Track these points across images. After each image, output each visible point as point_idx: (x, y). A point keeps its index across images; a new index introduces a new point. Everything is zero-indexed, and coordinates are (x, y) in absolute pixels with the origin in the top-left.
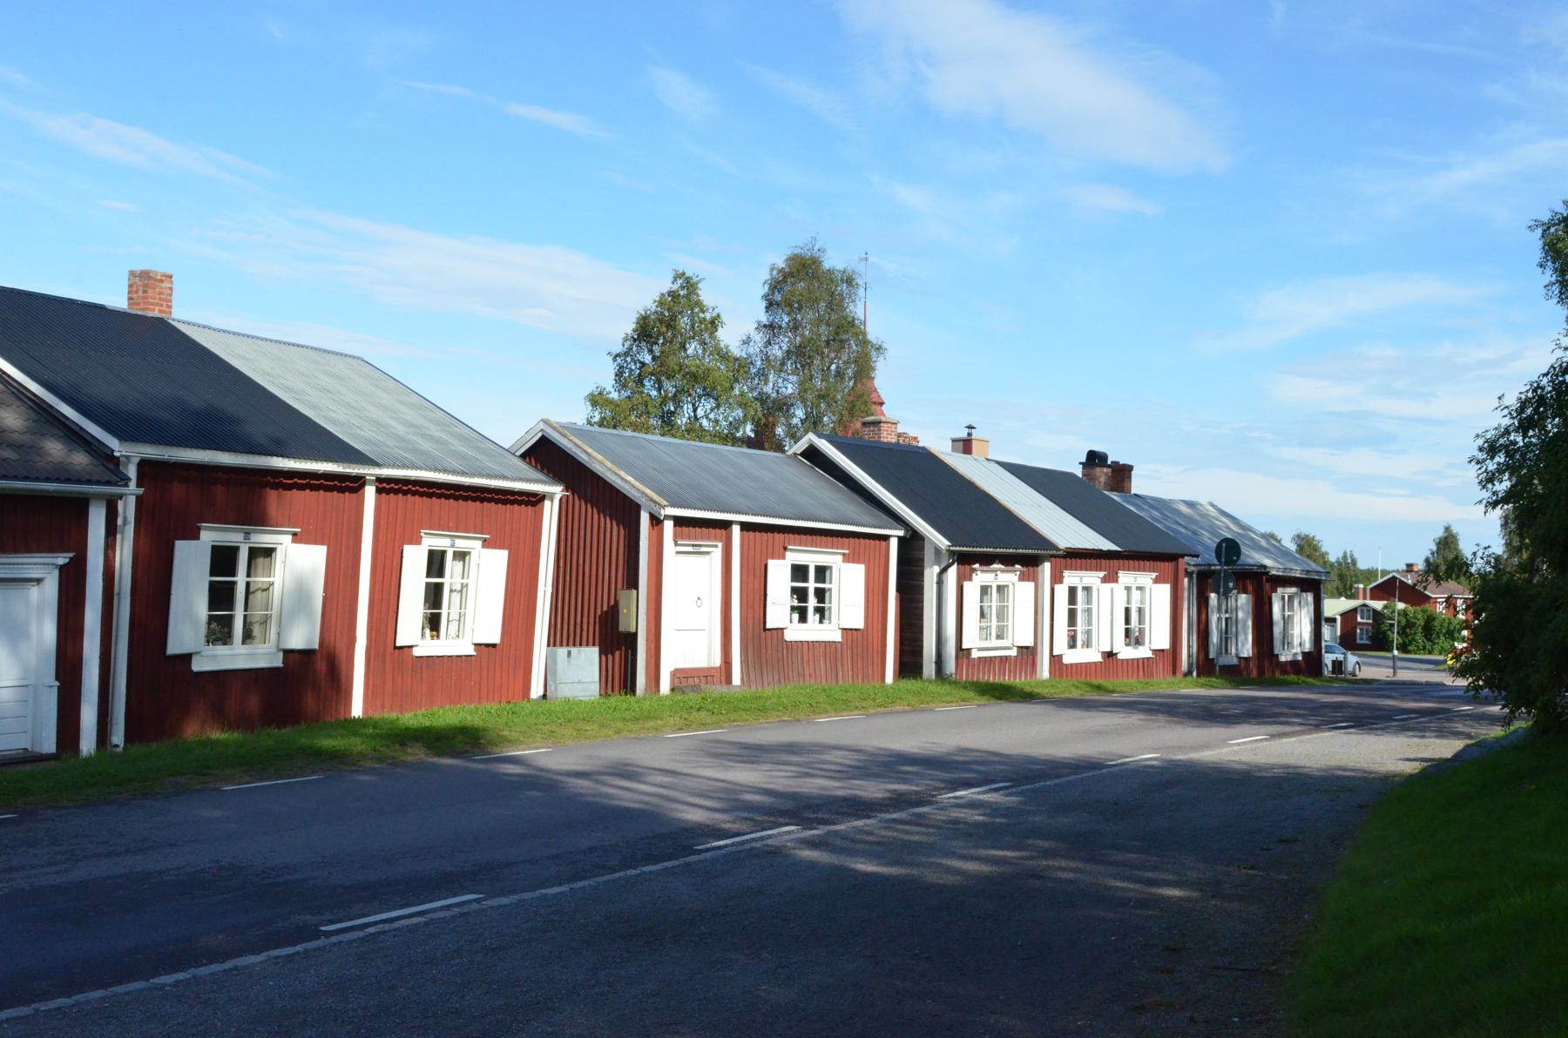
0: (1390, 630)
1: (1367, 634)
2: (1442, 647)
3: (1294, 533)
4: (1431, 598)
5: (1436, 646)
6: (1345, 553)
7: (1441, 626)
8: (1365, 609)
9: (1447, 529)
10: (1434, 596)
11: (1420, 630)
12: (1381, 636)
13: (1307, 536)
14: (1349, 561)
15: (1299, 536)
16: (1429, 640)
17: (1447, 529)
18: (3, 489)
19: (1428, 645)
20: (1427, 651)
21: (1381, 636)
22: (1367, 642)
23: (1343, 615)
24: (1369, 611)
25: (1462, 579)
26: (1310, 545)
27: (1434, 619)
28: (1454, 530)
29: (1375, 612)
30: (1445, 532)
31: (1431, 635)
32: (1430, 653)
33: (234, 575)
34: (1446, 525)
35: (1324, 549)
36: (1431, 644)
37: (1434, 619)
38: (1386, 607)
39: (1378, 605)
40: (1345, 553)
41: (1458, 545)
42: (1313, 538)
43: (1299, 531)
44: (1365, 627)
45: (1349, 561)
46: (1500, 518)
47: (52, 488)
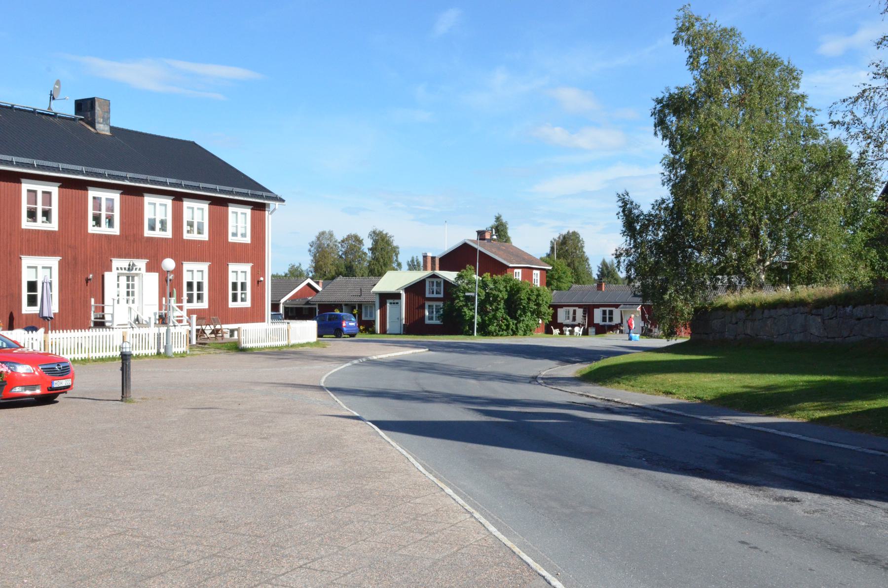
0: (466, 305)
1: (437, 312)
2: (527, 326)
3: (370, 229)
4: (508, 267)
5: (521, 325)
6: (413, 258)
7: (529, 299)
8: (435, 280)
9: (498, 219)
10: (511, 265)
11: (502, 305)
12: (721, 212)
13: (381, 232)
14: (416, 264)
15: (374, 232)
16: (514, 317)
17: (498, 219)
18: (884, 397)
19: (512, 322)
20: (510, 331)
21: (721, 212)
22: (438, 322)
23: (409, 289)
24: (438, 284)
25: (800, 77)
26: (383, 240)
27: (519, 290)
28: (504, 219)
29: (447, 283)
30: (496, 221)
31: (516, 312)
32: (515, 333)
33: (182, 303)
34: (497, 215)
35: (395, 244)
36: (515, 322)
37: (519, 290)
38: (460, 277)
39: (451, 276)
40: (413, 258)
41: (507, 233)
42: (386, 234)
43: (374, 228)
44: (434, 304)
45: (416, 264)
46: (653, 114)
47: (879, 401)
